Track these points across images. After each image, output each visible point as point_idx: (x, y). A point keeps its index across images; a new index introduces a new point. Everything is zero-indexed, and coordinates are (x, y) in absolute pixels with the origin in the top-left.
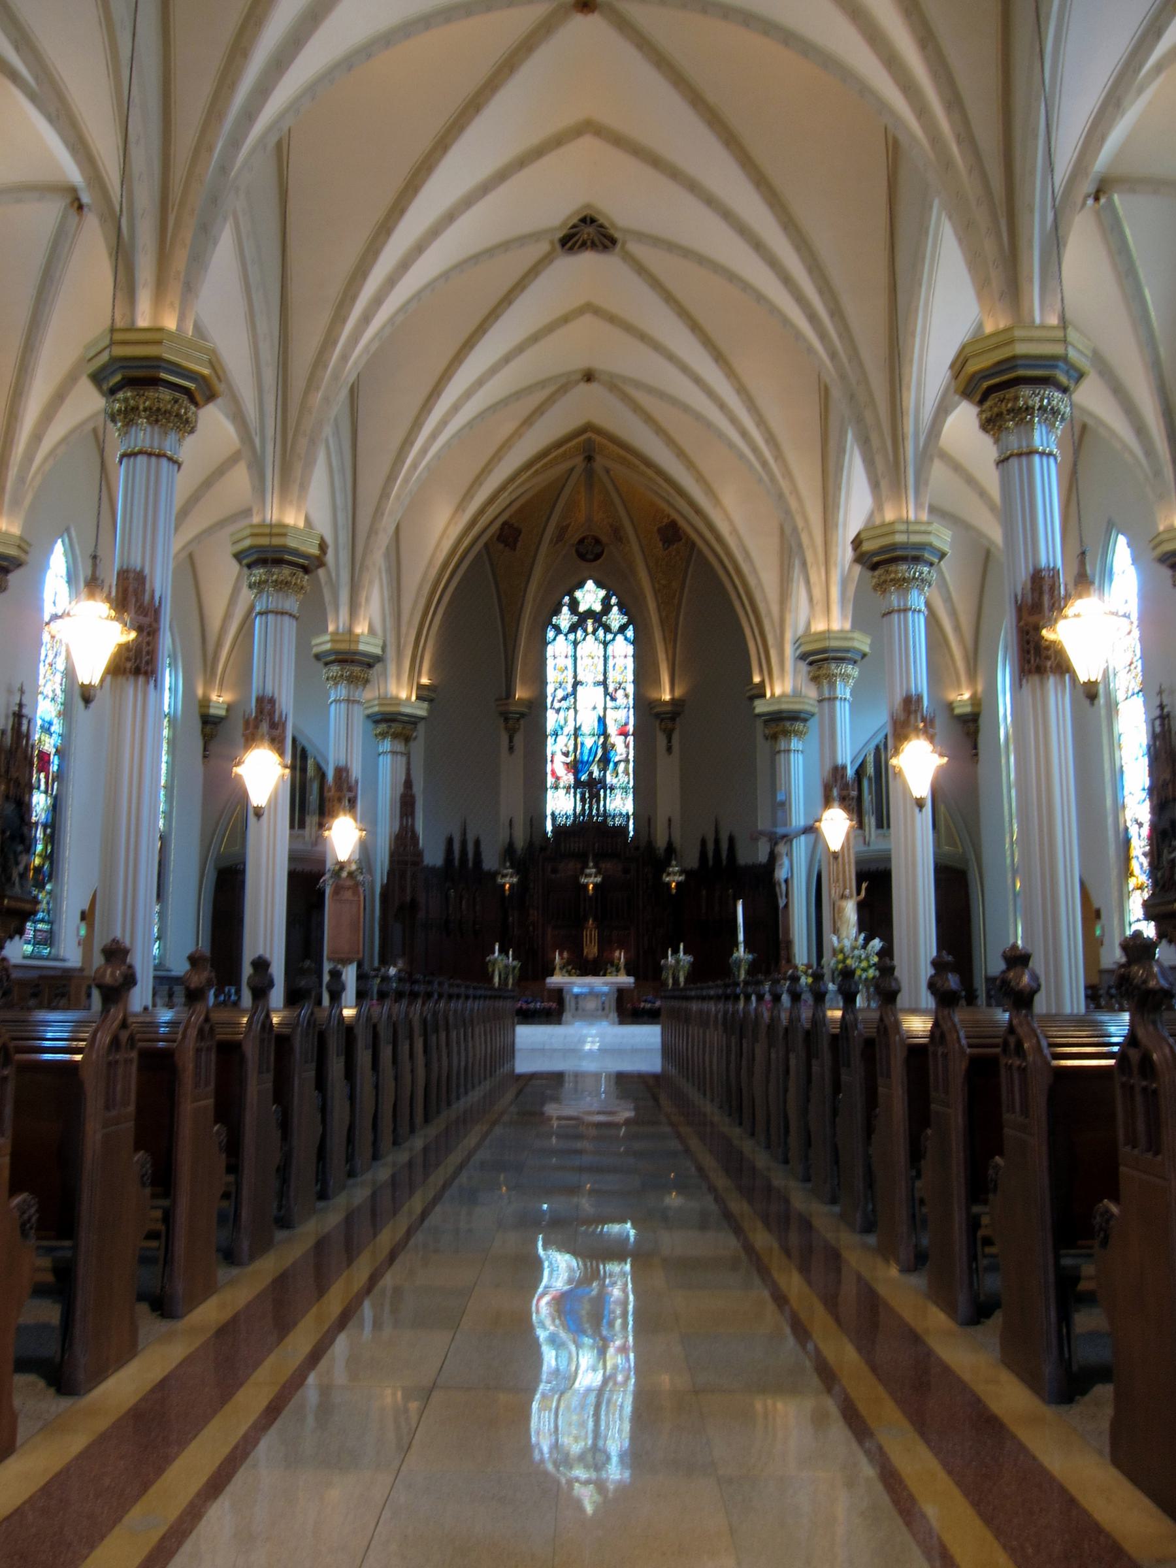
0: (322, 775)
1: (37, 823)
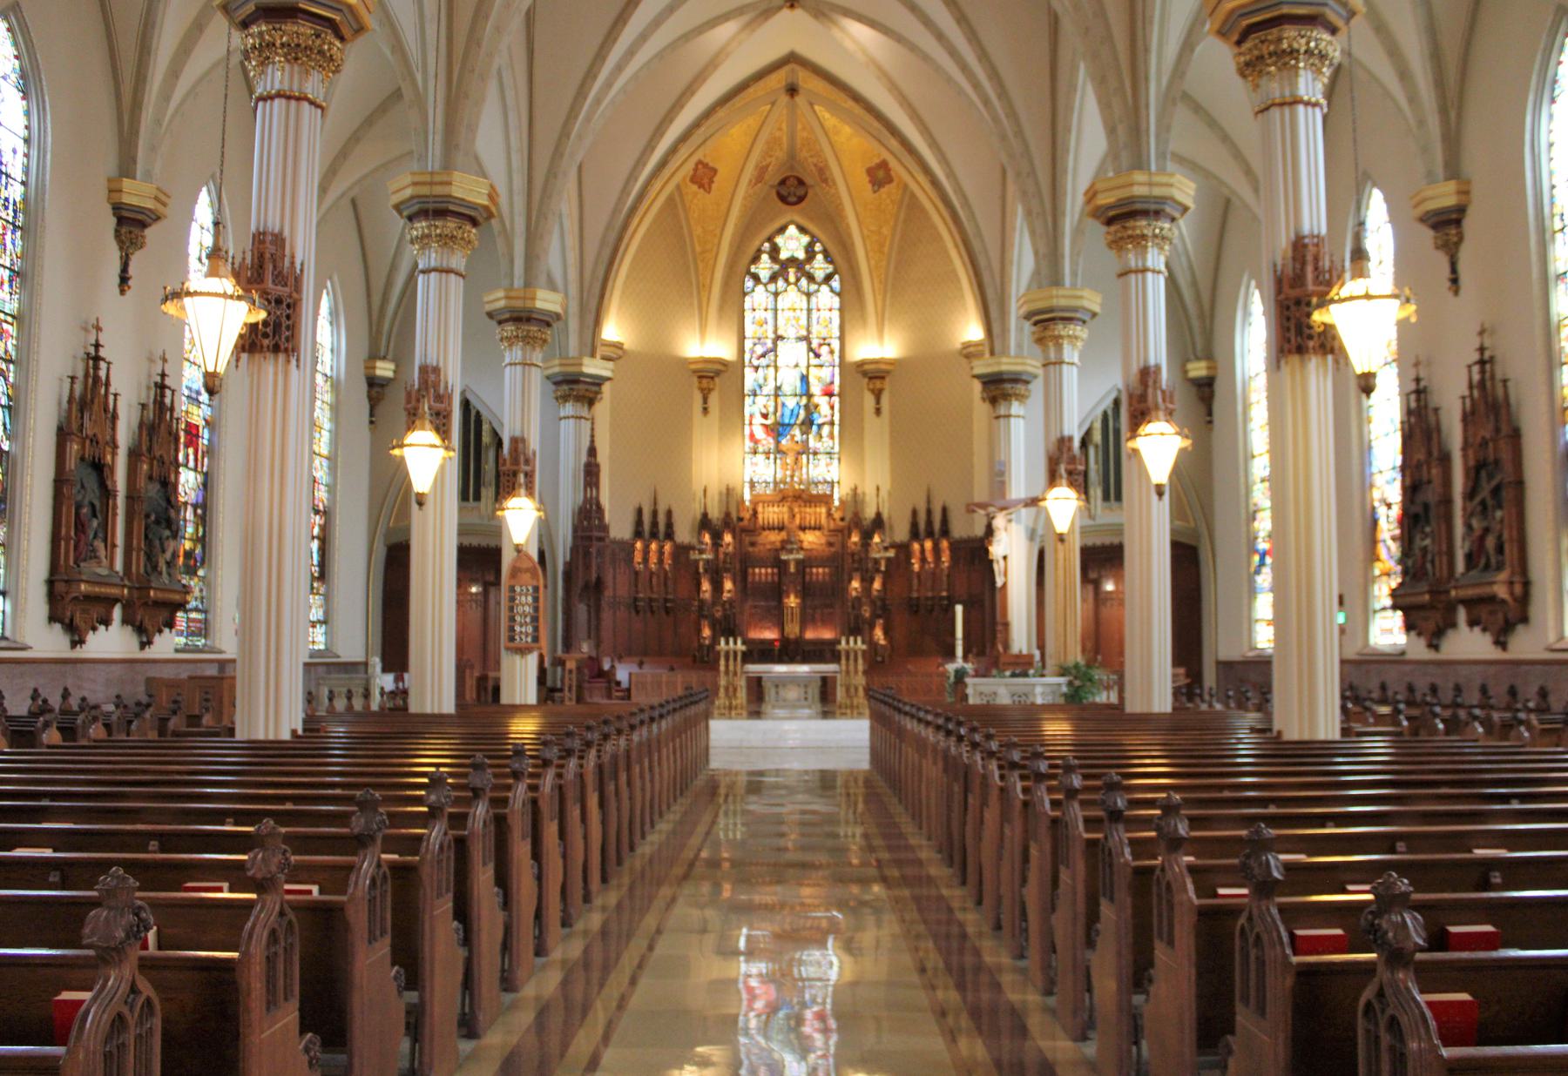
0: (499, 444)
1: (186, 504)
